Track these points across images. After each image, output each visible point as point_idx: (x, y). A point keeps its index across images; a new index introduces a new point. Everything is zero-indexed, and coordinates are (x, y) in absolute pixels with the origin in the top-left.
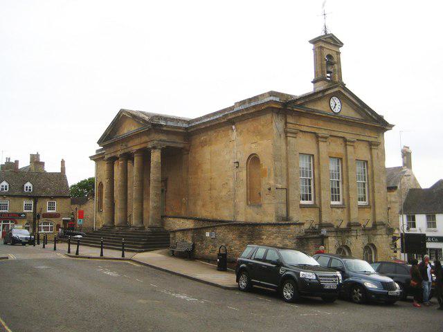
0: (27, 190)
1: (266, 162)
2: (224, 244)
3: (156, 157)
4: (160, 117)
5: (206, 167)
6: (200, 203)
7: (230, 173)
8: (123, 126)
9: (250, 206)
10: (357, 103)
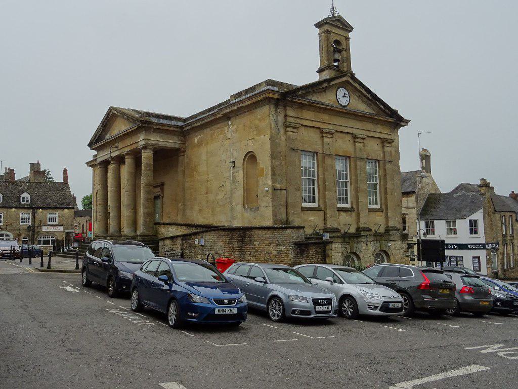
0: (23, 201)
1: (264, 161)
2: (213, 252)
4: (149, 114)
5: (202, 168)
6: (196, 208)
7: (226, 175)
8: (114, 126)
9: (248, 209)
10: (368, 95)
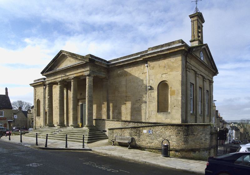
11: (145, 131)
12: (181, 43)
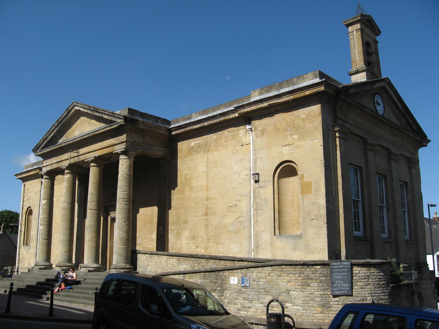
3: (124, 165)
11: (234, 280)
12: (318, 79)
